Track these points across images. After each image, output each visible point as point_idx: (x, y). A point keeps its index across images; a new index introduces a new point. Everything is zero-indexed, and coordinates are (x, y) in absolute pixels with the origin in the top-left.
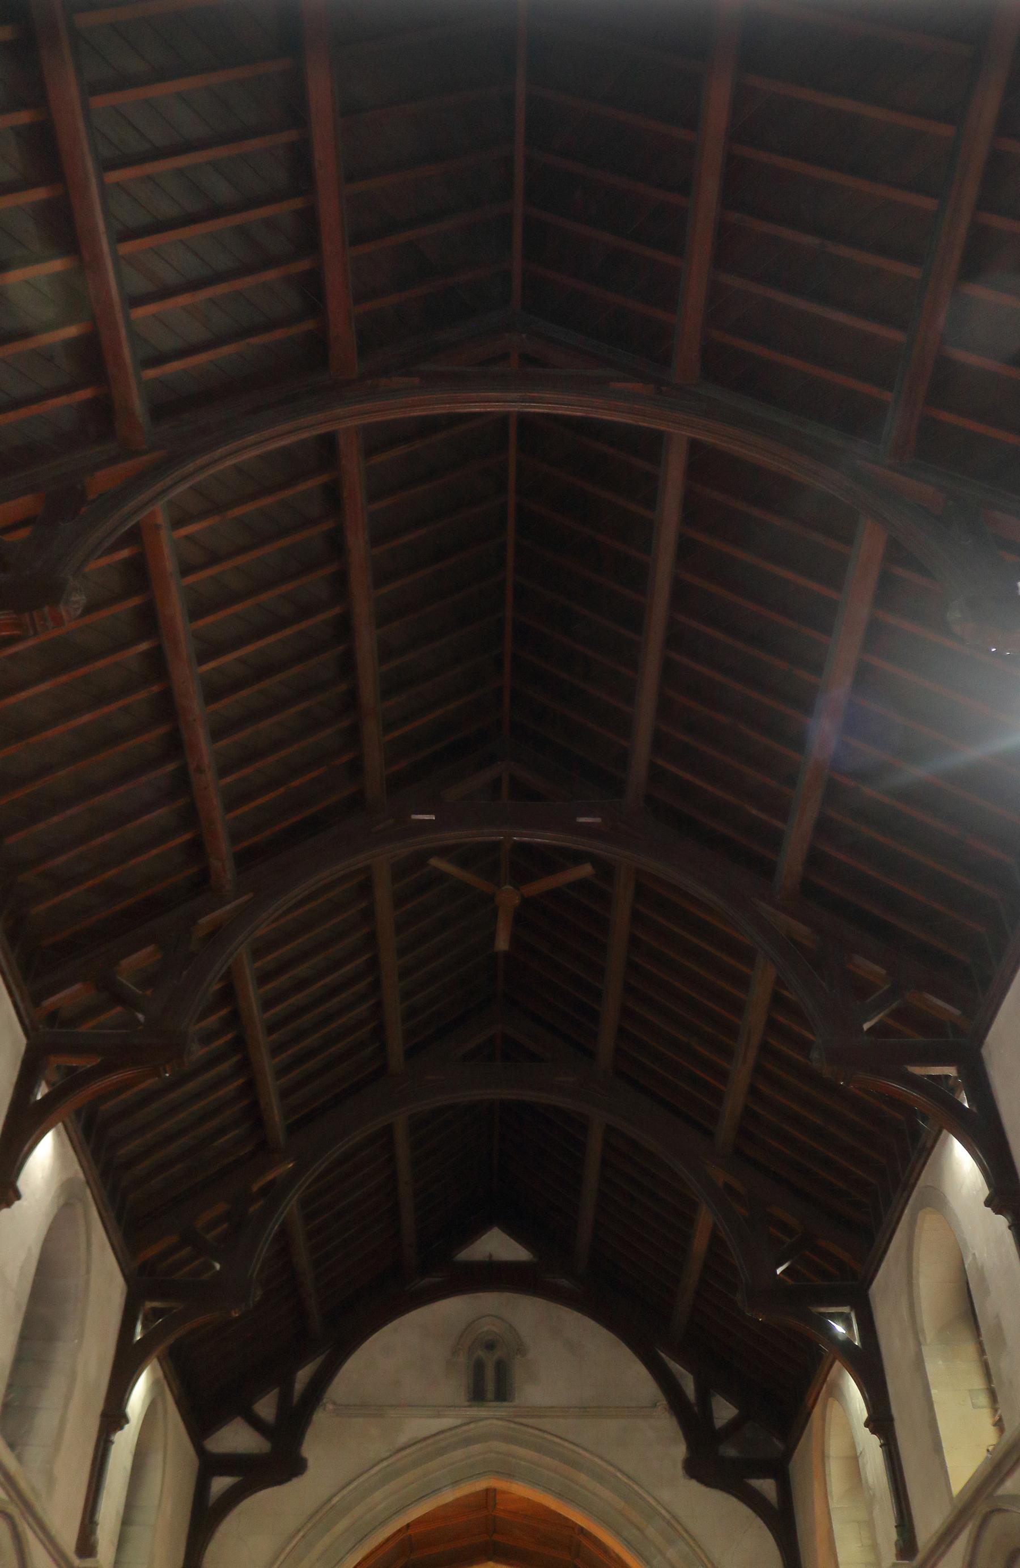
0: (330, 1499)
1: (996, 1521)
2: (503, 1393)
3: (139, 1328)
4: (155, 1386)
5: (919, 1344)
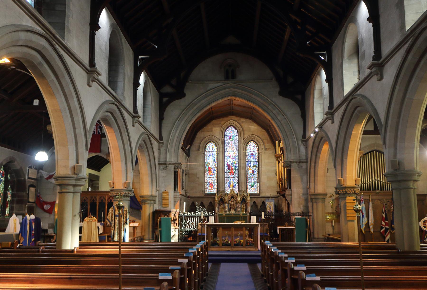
0: (192, 102)
1: (353, 101)
2: (233, 77)
3: (139, 63)
4: (145, 77)
5: (342, 60)
